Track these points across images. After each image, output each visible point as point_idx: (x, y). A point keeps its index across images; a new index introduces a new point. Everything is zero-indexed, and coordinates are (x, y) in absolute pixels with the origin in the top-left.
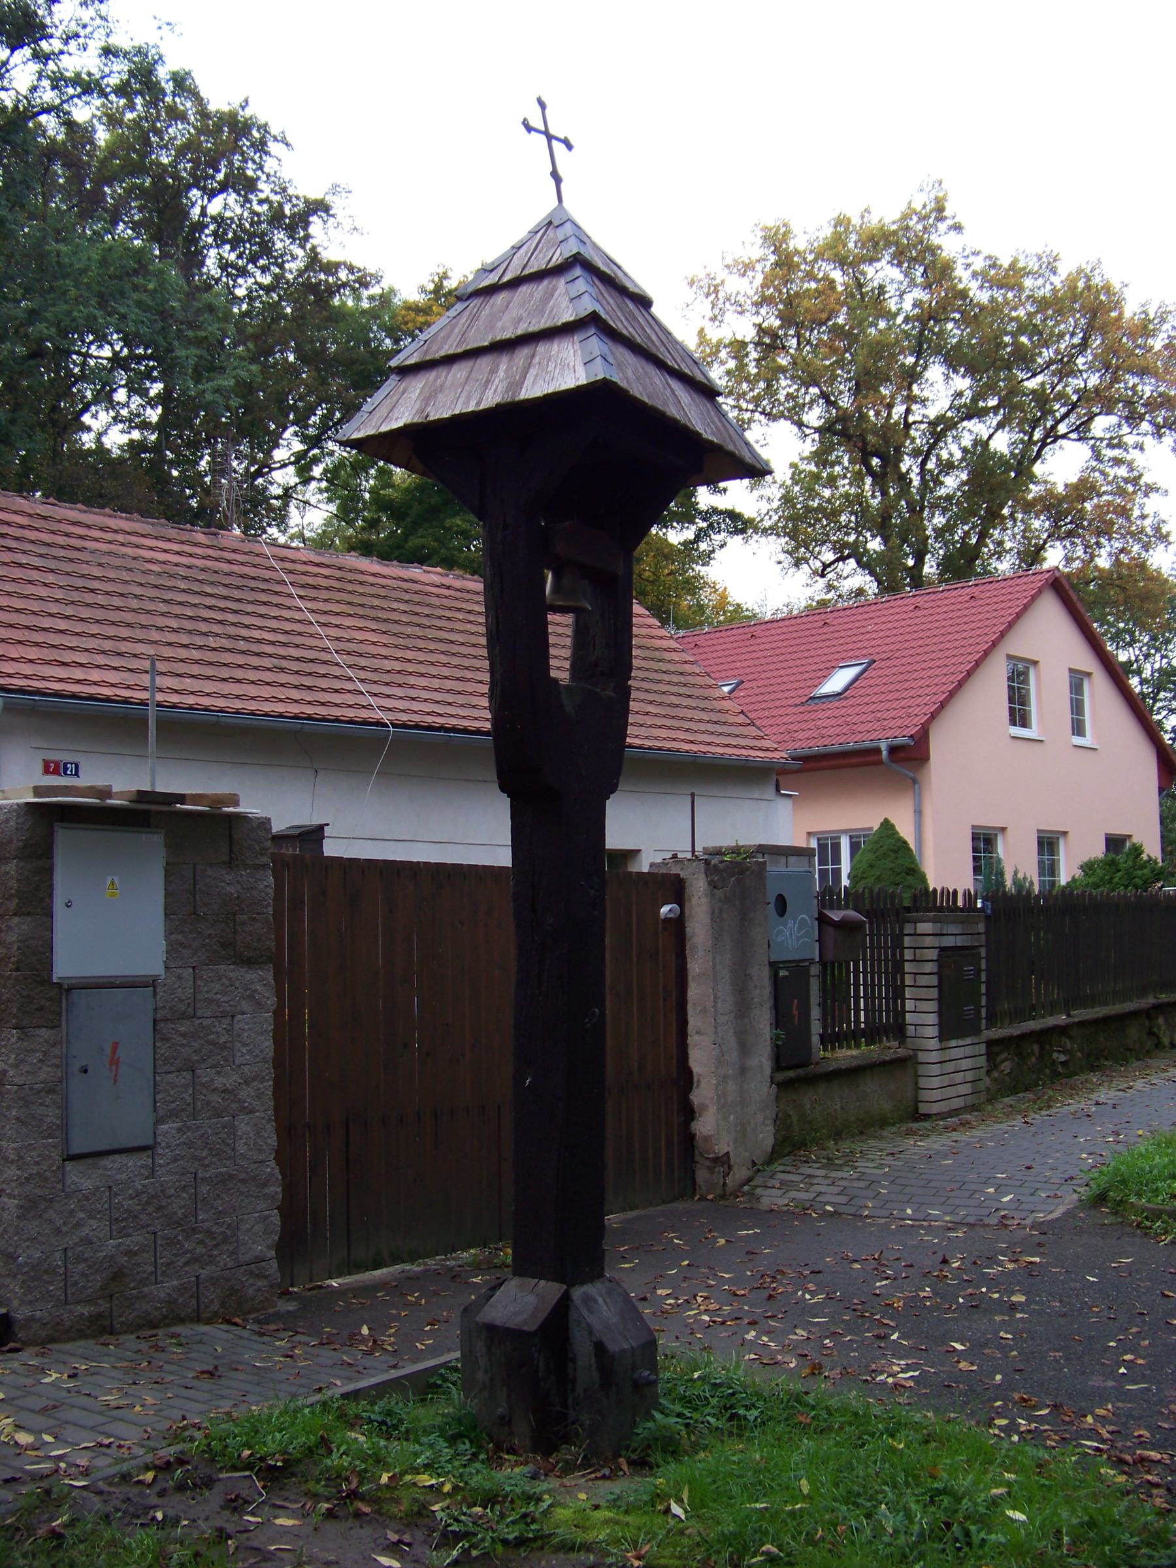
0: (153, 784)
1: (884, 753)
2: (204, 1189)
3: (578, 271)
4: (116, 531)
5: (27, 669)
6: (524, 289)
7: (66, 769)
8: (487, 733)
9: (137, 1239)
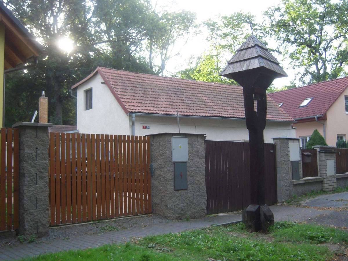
0: (133, 131)
1: (316, 119)
2: (195, 196)
3: (256, 47)
4: (152, 79)
5: (139, 108)
6: (249, 50)
7: (147, 127)
8: (244, 118)
9: (185, 204)
